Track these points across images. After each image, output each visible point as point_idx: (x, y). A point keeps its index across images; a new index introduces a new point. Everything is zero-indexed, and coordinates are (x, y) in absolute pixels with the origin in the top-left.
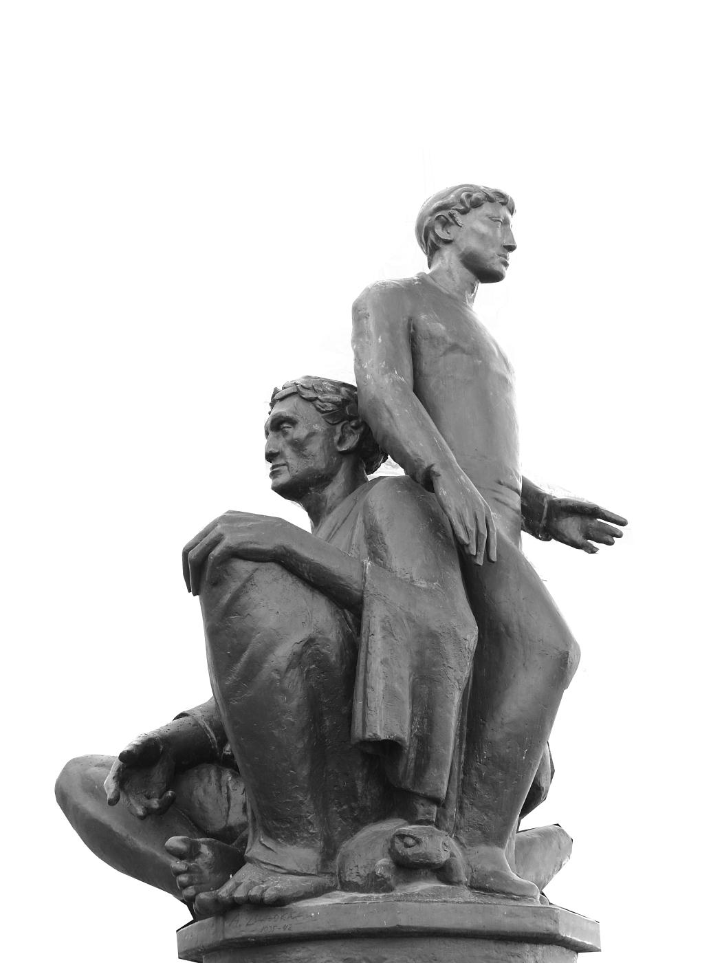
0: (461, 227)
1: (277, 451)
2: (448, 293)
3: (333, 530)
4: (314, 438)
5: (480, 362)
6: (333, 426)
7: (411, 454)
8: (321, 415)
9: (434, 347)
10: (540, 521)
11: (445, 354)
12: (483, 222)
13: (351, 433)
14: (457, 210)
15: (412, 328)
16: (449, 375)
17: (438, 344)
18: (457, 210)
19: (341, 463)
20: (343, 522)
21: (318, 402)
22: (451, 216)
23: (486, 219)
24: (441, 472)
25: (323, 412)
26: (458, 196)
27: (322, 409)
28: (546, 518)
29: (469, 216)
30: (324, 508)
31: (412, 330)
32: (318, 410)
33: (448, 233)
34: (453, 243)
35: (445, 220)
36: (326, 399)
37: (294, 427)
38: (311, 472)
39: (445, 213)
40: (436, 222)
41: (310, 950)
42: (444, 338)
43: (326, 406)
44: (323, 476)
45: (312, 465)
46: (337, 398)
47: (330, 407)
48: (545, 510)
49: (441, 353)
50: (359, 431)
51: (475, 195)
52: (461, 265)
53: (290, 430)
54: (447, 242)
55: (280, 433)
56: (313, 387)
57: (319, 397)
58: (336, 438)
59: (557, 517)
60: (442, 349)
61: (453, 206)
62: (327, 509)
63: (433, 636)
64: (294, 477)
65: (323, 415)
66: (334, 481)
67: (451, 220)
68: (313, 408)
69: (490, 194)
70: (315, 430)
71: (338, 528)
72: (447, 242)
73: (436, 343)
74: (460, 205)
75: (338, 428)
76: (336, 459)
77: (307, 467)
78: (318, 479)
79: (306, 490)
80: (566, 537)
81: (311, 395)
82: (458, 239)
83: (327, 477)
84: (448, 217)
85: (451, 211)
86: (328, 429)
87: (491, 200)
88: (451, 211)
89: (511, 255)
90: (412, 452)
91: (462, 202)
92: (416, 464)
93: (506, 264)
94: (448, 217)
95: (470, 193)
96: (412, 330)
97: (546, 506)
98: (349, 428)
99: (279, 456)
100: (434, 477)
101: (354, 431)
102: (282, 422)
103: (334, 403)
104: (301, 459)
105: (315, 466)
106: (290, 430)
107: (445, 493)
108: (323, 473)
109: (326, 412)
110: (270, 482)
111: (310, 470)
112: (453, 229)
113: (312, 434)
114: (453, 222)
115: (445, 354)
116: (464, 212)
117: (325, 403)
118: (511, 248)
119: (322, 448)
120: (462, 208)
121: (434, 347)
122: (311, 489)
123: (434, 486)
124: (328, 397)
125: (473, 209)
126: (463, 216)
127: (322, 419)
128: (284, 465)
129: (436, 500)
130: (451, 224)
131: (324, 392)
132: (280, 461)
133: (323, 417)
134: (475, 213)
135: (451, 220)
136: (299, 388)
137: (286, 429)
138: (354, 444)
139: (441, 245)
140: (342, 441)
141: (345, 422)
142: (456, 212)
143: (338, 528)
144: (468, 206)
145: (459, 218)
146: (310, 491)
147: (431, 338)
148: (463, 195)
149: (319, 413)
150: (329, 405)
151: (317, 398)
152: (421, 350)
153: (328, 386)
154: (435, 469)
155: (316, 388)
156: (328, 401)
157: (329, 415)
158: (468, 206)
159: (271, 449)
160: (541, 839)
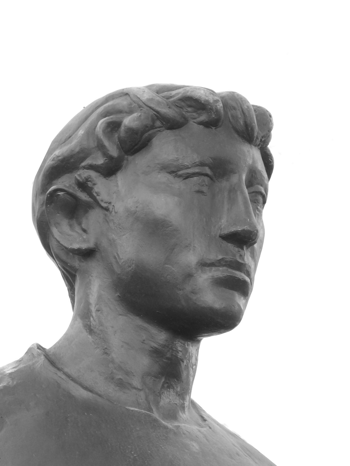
0: (107, 209)
33: (85, 231)
34: (98, 255)
35: (68, 198)
41: (207, 274)
61: (84, 159)
63: (96, 310)
67: (83, 196)
82: (104, 243)
93: (172, 175)
123: (247, 443)
125: (130, 158)
129: (59, 265)
130: (87, 207)
135: (83, 196)
142: (93, 174)
144: (114, 152)
160: (265, 138)
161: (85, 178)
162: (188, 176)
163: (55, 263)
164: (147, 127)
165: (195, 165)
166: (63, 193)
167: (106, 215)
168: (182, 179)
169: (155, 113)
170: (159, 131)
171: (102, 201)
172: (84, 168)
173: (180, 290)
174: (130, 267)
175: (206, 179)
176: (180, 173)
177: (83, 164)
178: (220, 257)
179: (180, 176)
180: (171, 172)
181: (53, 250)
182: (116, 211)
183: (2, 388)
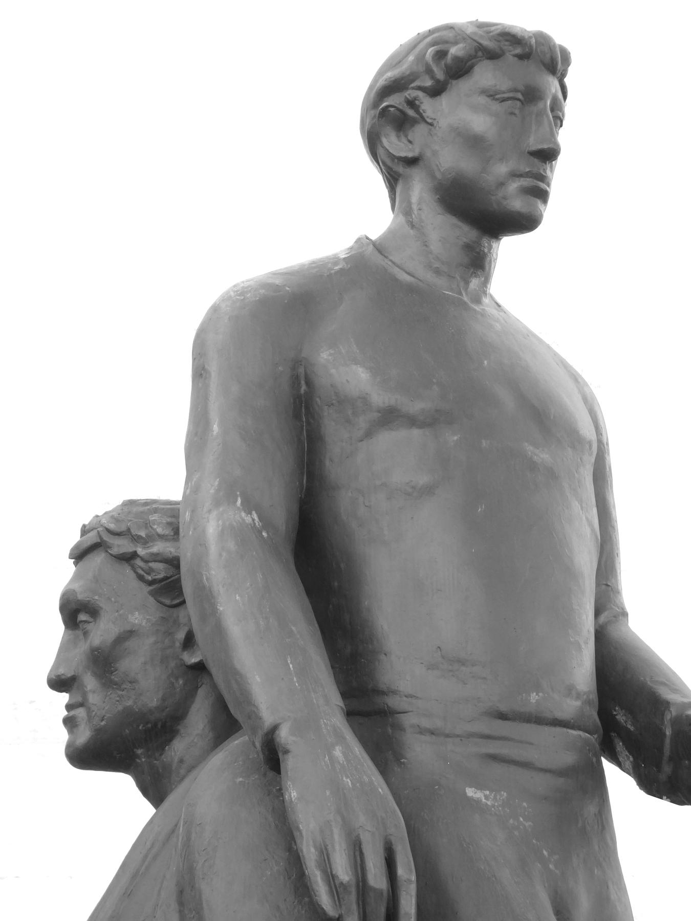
0: (431, 125)
2: (408, 278)
4: (131, 644)
9: (348, 421)
10: (659, 767)
11: (369, 434)
12: (475, 108)
14: (420, 88)
15: (303, 382)
22: (411, 103)
23: (483, 100)
25: (150, 583)
26: (421, 58)
28: (671, 759)
29: (444, 101)
31: (304, 388)
32: (141, 578)
33: (410, 142)
34: (421, 163)
35: (398, 113)
36: (152, 554)
37: (95, 621)
38: (130, 717)
39: (395, 100)
48: (668, 741)
51: (454, 51)
55: (79, 633)
56: (129, 530)
60: (362, 422)
61: (413, 81)
65: (151, 588)
66: (182, 731)
67: (411, 113)
68: (132, 575)
69: (482, 42)
72: (412, 162)
73: (350, 412)
76: (181, 682)
77: (120, 708)
81: (122, 546)
82: (428, 154)
83: (164, 726)
87: (492, 55)
88: (411, 94)
96: (304, 388)
97: (668, 732)
100: (280, 755)
111: (128, 713)
112: (418, 133)
116: (436, 91)
117: (152, 565)
121: (348, 421)
122: (139, 751)
124: (155, 550)
125: (454, 82)
130: (413, 122)
134: (463, 86)
135: (411, 113)
136: (102, 533)
142: (420, 94)
145: (428, 106)
149: (143, 585)
156: (156, 557)
159: (61, 671)
162: (503, 100)
164: (471, 56)
165: (510, 91)
168: (498, 102)
170: (480, 60)
171: (428, 117)
172: (413, 88)
173: (493, 195)
175: (518, 103)
176: (497, 96)
177: (412, 85)
178: (528, 170)
179: (497, 99)
180: (490, 96)
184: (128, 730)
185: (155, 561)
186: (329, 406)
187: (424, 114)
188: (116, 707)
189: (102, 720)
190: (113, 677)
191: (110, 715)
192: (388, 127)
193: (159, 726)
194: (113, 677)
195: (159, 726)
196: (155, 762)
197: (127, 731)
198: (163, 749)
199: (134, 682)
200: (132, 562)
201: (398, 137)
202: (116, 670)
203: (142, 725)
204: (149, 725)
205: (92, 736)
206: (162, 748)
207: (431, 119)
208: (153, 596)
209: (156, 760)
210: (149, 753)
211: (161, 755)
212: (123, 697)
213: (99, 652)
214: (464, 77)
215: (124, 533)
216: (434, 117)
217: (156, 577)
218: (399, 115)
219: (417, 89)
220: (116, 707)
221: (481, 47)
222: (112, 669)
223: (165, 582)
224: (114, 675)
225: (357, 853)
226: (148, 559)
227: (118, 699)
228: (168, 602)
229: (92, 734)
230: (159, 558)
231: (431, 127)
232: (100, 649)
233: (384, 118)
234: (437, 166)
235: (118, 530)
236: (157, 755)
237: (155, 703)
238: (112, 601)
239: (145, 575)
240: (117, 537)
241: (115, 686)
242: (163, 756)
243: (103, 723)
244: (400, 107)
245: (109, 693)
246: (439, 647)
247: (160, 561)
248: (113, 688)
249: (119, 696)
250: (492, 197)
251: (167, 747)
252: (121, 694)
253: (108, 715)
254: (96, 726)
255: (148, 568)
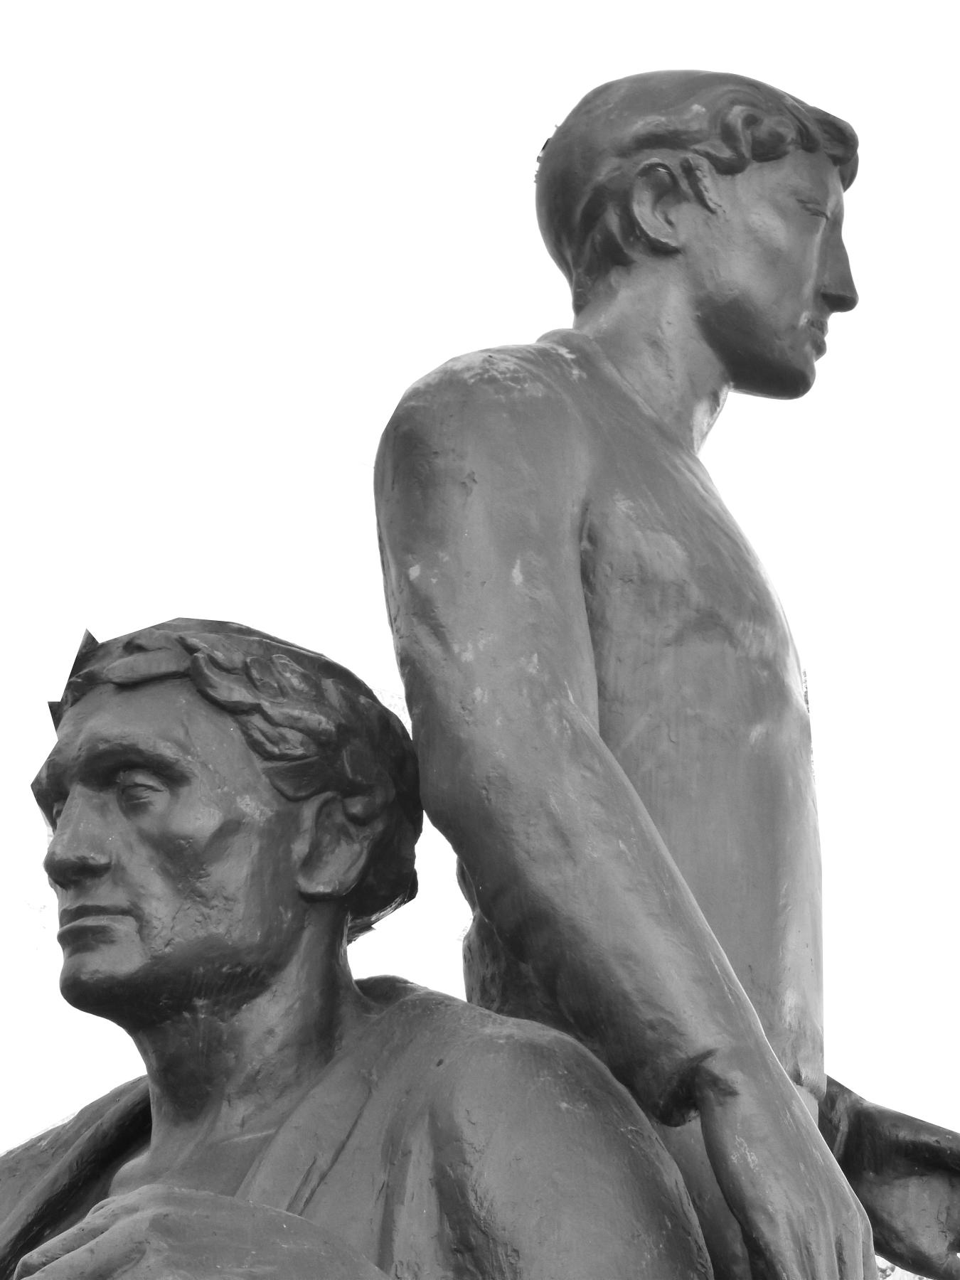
0: (712, 211)
1: (102, 860)
3: (306, 1180)
4: (238, 842)
5: (765, 673)
6: (291, 805)
7: (635, 998)
8: (260, 764)
9: (652, 611)
11: (679, 639)
13: (343, 833)
14: (708, 156)
16: (689, 712)
17: (662, 602)
18: (708, 156)
19: (302, 928)
20: (335, 1160)
21: (257, 720)
22: (689, 170)
24: (736, 1078)
25: (268, 756)
27: (269, 747)
30: (228, 1073)
32: (255, 745)
33: (670, 223)
34: (680, 257)
35: (667, 179)
38: (211, 951)
39: (666, 158)
40: (640, 182)
42: (681, 589)
43: (284, 739)
44: (249, 970)
45: (221, 930)
46: (320, 721)
47: (295, 745)
49: (670, 634)
50: (368, 831)
52: (693, 329)
53: (159, 800)
54: (661, 251)
55: (110, 797)
57: (266, 705)
58: (300, 848)
59: (877, 1172)
61: (698, 141)
62: (240, 1078)
64: (157, 960)
65: (269, 764)
67: (684, 185)
70: (244, 815)
71: (323, 1177)
72: (661, 251)
74: (718, 142)
75: (308, 812)
77: (202, 933)
78: (231, 977)
79: (182, 1003)
80: (900, 1239)
83: (256, 975)
84: (678, 172)
85: (690, 155)
86: (278, 814)
87: (807, 143)
89: (836, 320)
90: (640, 990)
91: (728, 135)
92: (649, 1033)
94: (678, 172)
95: (757, 113)
98: (339, 818)
99: (106, 877)
101: (352, 829)
102: (133, 766)
103: (311, 734)
104: (188, 904)
105: (228, 931)
106: (159, 800)
107: (752, 1158)
108: (249, 960)
109: (282, 757)
110: (54, 960)
111: (211, 943)
113: (230, 828)
114: (690, 192)
115: (679, 639)
116: (728, 169)
118: (842, 299)
119: (256, 875)
120: (726, 153)
122: (200, 1003)
125: (755, 165)
126: (724, 181)
127: (264, 779)
128: (124, 912)
130: (680, 197)
131: (282, 692)
132: (105, 894)
133: (268, 772)
135: (684, 185)
137: (147, 795)
138: (354, 874)
139: (636, 255)
140: (311, 862)
141: (329, 794)
142: (705, 164)
143: (323, 1177)
144: (745, 150)
145: (711, 184)
146: (193, 1010)
147: (644, 581)
148: (737, 114)
149: (254, 756)
150: (291, 734)
151: (257, 709)
152: (609, 615)
153: (293, 672)
154: (716, 1066)
155: (255, 674)
156: (294, 723)
157: (288, 770)
158: (747, 155)
161: (150, 803)
163: (383, 916)
166: (664, 170)
167: (709, 218)
168: (809, 213)
169: (802, 127)
171: (711, 200)
172: (696, 152)
173: (779, 339)
174: (732, 290)
176: (810, 206)
177: (697, 147)
179: (808, 209)
180: (801, 201)
181: (863, 1214)
182: (728, 218)
183: (72, 887)
184: (204, 969)
185: (292, 728)
186: (626, 582)
187: (705, 193)
188: (195, 931)
189: (167, 945)
190: (198, 884)
191: (182, 940)
192: (646, 192)
193: (250, 975)
194: (198, 884)
195: (250, 975)
196: (221, 1023)
197: (201, 969)
198: (239, 1008)
199: (232, 900)
200: (244, 718)
201: (654, 208)
202: (208, 875)
203: (228, 966)
204: (239, 969)
205: (147, 964)
206: (237, 1006)
207: (715, 204)
208: (268, 776)
209: (223, 1020)
210: (217, 1008)
211: (233, 1015)
212: (210, 919)
213: (189, 842)
214: (771, 162)
215: (237, 671)
216: (719, 203)
217: (289, 752)
218: (667, 182)
219: (701, 155)
220: (195, 931)
221: (802, 127)
222: (202, 872)
223: (299, 762)
224: (201, 882)
225: (805, 1252)
226: (281, 723)
227: (200, 918)
228: (290, 792)
229: (146, 961)
230: (301, 725)
231: (710, 214)
232: (191, 839)
233: (645, 178)
234: (711, 271)
235: (227, 664)
236: (227, 1013)
237: (258, 939)
238: (209, 769)
239: (267, 742)
240: (224, 673)
241: (198, 899)
242: (235, 1018)
243: (167, 950)
244: (675, 173)
245: (187, 907)
246: (750, 966)
247: (300, 730)
248: (195, 901)
249: (203, 915)
250: (777, 341)
251: (245, 1005)
252: (208, 914)
253: (177, 940)
254: (156, 951)
255: (276, 734)
